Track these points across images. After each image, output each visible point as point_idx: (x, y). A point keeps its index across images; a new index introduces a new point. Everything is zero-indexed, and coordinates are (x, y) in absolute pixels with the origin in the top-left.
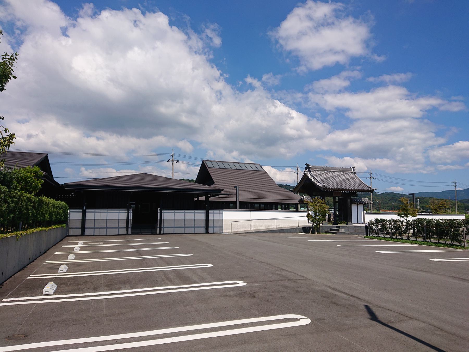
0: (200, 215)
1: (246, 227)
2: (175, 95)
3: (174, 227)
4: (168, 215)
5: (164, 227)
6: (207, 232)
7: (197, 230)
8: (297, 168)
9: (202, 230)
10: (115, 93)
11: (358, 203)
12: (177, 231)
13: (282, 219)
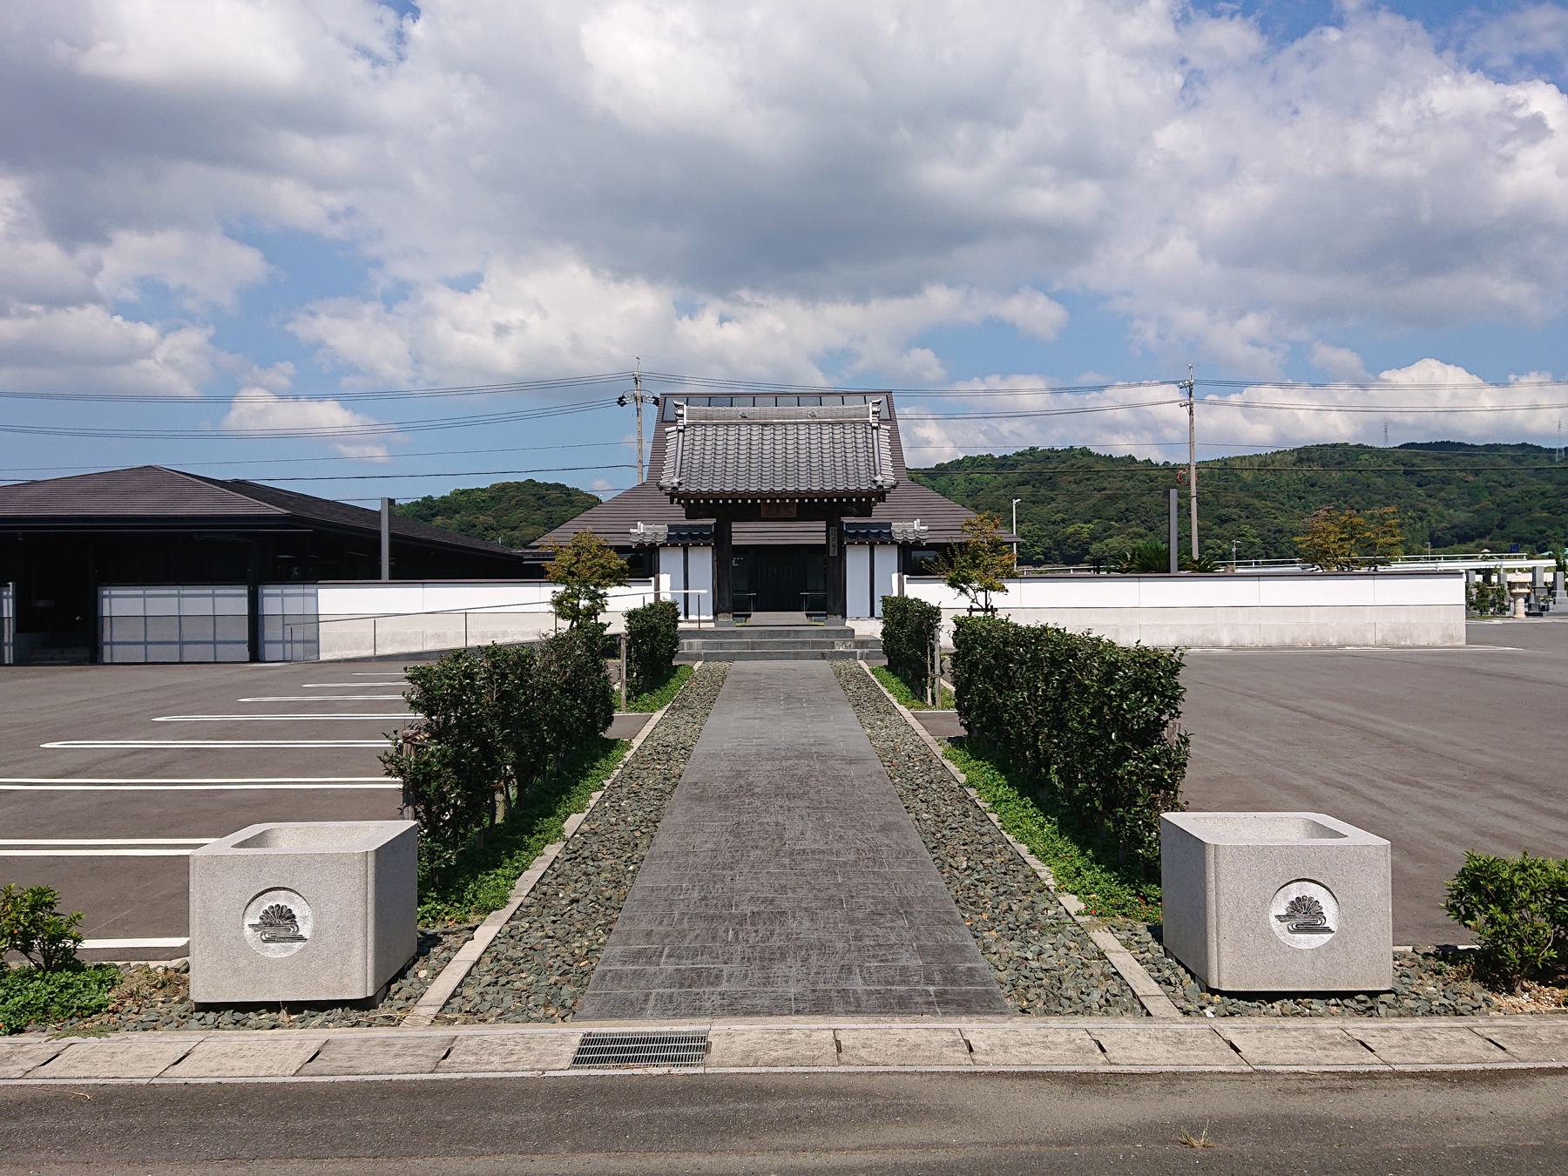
0: (231, 602)
1: (403, 642)
2: (981, 105)
3: (146, 643)
4: (122, 605)
5: (112, 644)
6: (256, 656)
7: (224, 652)
8: (1191, 385)
9: (243, 652)
10: (763, 134)
11: (877, 537)
12: (156, 653)
13: (495, 612)
